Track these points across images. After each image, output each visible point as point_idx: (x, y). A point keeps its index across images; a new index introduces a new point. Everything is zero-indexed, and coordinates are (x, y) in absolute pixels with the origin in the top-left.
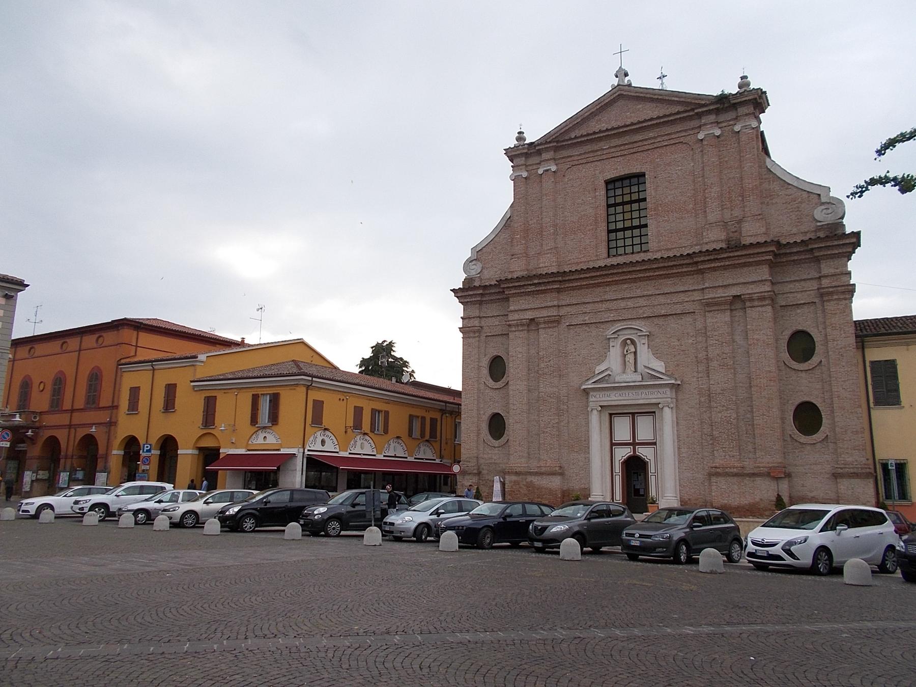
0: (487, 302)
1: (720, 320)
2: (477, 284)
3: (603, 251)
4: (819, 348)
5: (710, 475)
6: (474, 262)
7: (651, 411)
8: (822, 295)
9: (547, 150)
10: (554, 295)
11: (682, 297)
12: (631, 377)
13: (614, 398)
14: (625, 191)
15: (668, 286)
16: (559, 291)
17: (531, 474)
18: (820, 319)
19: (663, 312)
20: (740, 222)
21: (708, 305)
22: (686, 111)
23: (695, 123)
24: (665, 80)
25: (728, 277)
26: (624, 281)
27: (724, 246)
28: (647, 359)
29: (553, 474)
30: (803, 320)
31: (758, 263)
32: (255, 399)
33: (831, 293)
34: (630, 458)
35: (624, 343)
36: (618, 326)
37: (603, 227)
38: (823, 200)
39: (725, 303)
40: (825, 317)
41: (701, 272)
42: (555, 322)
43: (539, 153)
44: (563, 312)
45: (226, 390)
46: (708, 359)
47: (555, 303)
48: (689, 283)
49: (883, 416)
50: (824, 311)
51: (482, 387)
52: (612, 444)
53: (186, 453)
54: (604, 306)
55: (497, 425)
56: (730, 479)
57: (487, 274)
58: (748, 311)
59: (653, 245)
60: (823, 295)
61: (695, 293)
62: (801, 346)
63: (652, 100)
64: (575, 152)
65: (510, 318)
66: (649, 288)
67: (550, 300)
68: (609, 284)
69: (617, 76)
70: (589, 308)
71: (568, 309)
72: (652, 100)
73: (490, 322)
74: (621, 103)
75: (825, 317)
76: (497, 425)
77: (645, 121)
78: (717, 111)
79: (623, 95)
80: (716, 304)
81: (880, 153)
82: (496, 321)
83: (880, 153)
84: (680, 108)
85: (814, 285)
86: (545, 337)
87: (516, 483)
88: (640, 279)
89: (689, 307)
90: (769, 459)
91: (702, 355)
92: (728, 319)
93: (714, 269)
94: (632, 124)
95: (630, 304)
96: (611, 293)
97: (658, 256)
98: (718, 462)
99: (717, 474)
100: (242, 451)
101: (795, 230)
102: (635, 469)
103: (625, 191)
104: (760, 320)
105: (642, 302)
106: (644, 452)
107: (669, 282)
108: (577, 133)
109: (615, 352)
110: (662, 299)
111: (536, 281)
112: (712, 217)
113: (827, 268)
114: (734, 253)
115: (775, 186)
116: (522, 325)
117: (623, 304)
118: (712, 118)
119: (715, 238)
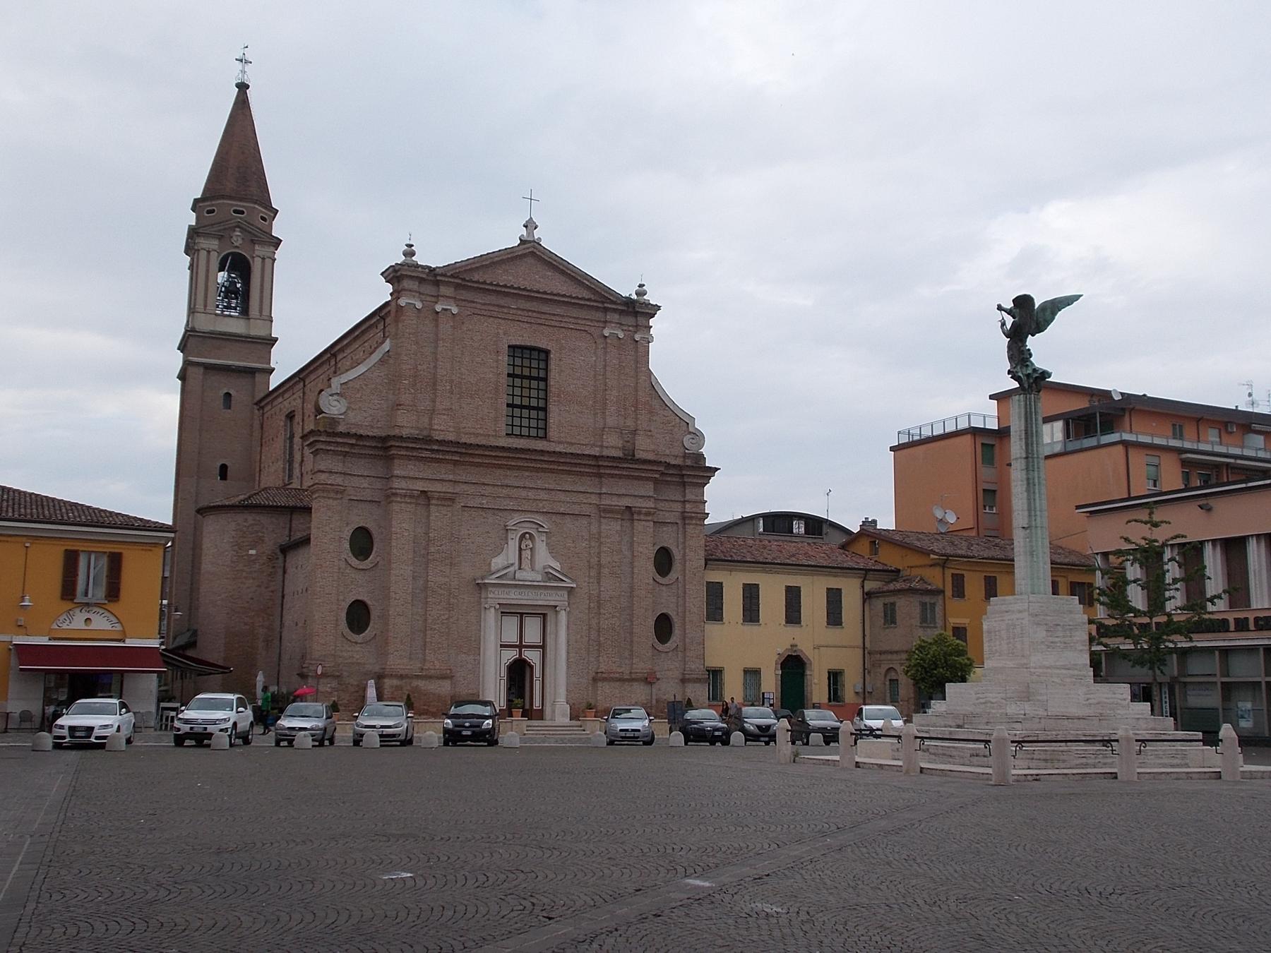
1: (612, 527)
2: (341, 429)
3: (503, 429)
4: (677, 566)
5: (595, 680)
6: (336, 397)
8: (684, 518)
9: (448, 284)
10: (450, 467)
11: (581, 497)
12: (527, 575)
13: (514, 597)
14: (530, 365)
15: (568, 483)
16: (455, 463)
17: (418, 677)
18: (681, 540)
19: (562, 510)
20: (634, 432)
21: (604, 511)
22: (589, 300)
23: (599, 315)
24: (248, 68)
25: (621, 487)
26: (527, 469)
27: (619, 454)
28: (544, 557)
29: (443, 677)
30: (668, 538)
31: (647, 479)
32: (71, 560)
33: (691, 518)
34: (516, 661)
35: (523, 536)
36: (518, 518)
37: (505, 399)
38: (691, 429)
39: (617, 512)
40: (685, 537)
41: (600, 476)
42: (449, 500)
43: (437, 283)
44: (458, 489)
46: (600, 565)
47: (451, 477)
48: (587, 485)
49: (712, 629)
51: (343, 565)
52: (543, 647)
56: (613, 684)
57: (354, 418)
58: (636, 523)
59: (553, 433)
61: (593, 496)
62: (664, 561)
63: (563, 273)
64: (480, 298)
65: (396, 484)
66: (549, 481)
67: (444, 472)
68: (510, 468)
69: (526, 226)
70: (489, 490)
72: (563, 273)
73: (356, 482)
74: (530, 260)
75: (685, 537)
76: (358, 616)
77: (558, 295)
78: (621, 312)
80: (611, 511)
81: (243, 87)
82: (365, 483)
83: (243, 87)
84: (586, 294)
85: (678, 507)
86: (438, 515)
88: (544, 470)
89: (586, 510)
90: (641, 667)
91: (594, 560)
92: (619, 528)
93: (612, 476)
94: (545, 293)
95: (531, 494)
96: (512, 478)
98: (603, 668)
99: (604, 679)
100: (43, 641)
101: (668, 452)
102: (518, 674)
103: (530, 365)
104: (644, 529)
105: (543, 495)
106: (532, 656)
107: (570, 478)
108: (476, 277)
109: (513, 545)
110: (562, 497)
111: (435, 447)
112: (611, 421)
114: (627, 464)
115: (655, 403)
116: (411, 497)
117: (523, 493)
118: (616, 317)
119: (613, 445)
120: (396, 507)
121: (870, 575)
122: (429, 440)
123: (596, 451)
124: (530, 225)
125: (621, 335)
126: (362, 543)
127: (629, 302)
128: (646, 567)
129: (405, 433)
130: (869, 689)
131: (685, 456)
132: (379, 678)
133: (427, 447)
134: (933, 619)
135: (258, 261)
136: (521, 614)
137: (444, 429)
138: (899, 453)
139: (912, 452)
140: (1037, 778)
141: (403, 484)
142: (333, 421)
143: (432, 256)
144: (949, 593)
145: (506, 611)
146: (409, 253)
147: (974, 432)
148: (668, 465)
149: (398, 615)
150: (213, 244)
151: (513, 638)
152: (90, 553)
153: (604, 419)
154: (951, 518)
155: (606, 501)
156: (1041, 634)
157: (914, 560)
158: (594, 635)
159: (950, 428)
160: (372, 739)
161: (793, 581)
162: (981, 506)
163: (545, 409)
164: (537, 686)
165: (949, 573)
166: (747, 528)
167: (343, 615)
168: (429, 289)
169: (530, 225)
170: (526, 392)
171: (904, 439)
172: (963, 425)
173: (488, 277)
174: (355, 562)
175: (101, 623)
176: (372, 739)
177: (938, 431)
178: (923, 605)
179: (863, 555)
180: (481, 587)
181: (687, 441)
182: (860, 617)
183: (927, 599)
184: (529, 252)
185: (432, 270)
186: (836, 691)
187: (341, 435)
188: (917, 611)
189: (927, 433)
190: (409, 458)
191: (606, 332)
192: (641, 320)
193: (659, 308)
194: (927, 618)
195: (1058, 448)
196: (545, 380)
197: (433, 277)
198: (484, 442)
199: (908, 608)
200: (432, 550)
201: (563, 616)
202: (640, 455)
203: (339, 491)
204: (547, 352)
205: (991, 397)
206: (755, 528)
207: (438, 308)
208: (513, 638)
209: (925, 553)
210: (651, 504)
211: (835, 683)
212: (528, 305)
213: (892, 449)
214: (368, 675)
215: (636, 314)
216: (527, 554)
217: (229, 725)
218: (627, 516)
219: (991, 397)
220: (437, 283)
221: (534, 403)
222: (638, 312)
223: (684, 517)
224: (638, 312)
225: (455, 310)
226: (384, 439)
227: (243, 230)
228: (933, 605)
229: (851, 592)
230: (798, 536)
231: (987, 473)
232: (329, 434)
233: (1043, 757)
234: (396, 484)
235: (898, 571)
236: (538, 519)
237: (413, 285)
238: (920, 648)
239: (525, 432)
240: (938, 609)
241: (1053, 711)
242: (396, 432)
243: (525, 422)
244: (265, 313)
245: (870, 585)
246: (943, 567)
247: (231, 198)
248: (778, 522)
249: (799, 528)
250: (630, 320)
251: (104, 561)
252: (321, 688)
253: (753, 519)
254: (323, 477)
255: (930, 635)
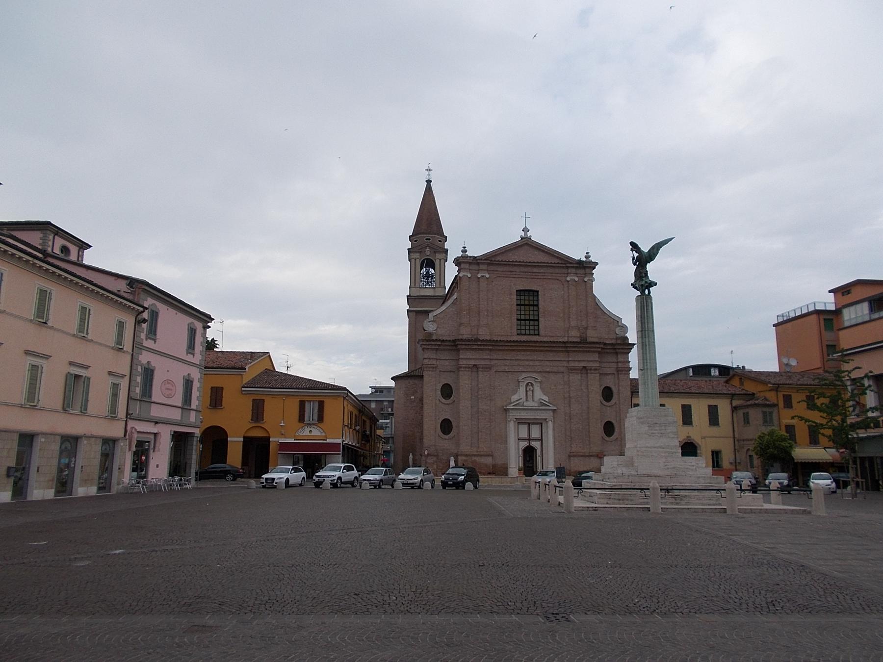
0: (441, 350)
1: (576, 378)
2: (434, 338)
3: (515, 332)
4: (615, 396)
5: (570, 456)
7: (540, 423)
9: (483, 263)
12: (530, 404)
13: (523, 415)
14: (528, 300)
15: (551, 356)
17: (475, 455)
20: (586, 328)
21: (571, 369)
23: (565, 271)
25: (580, 357)
27: (578, 340)
28: (539, 394)
30: (610, 382)
31: (594, 352)
32: (302, 405)
35: (527, 384)
36: (524, 375)
37: (515, 317)
41: (568, 352)
42: (488, 368)
45: (273, 395)
46: (570, 397)
48: (562, 356)
50: (618, 379)
52: (541, 440)
53: (235, 442)
54: (517, 363)
55: (446, 426)
57: (440, 332)
59: (542, 332)
60: (619, 371)
62: (607, 394)
63: (543, 251)
64: (500, 269)
65: (461, 362)
68: (519, 351)
70: (508, 362)
71: (496, 362)
72: (543, 251)
74: (526, 247)
76: (446, 426)
78: (577, 268)
79: (526, 243)
81: (429, 182)
83: (429, 182)
84: (557, 261)
85: (614, 365)
86: (483, 376)
87: (466, 461)
88: (537, 351)
89: (561, 369)
90: (595, 449)
91: (567, 395)
93: (574, 351)
95: (531, 363)
97: (545, 340)
98: (574, 450)
99: (574, 456)
100: (292, 441)
102: (529, 453)
103: (528, 300)
104: (594, 378)
105: (537, 363)
106: (536, 445)
108: (498, 258)
109: (522, 389)
110: (548, 363)
112: (573, 323)
113: (621, 358)
114: (583, 345)
117: (527, 363)
118: (573, 270)
119: (574, 335)
120: (461, 373)
121: (735, 397)
122: (477, 340)
123: (566, 339)
124: (526, 230)
125: (577, 279)
126: (447, 391)
127: (580, 262)
128: (596, 396)
129: (465, 337)
130: (738, 461)
131: (617, 339)
132: (456, 457)
133: (476, 344)
134: (771, 420)
135: (438, 261)
136: (529, 423)
137: (484, 334)
138: (780, 327)
139: (786, 327)
140: (596, 509)
141: (465, 362)
142: (430, 334)
143: (475, 251)
144: (781, 404)
145: (520, 422)
146: (464, 251)
147: (818, 312)
148: (605, 344)
149: (464, 425)
150: (417, 255)
151: (526, 436)
152: (310, 401)
153: (569, 322)
154: (793, 363)
155: (572, 364)
156: (645, 428)
157: (761, 388)
158: (568, 434)
159: (805, 311)
160: (327, 484)
161: (686, 401)
162: (825, 354)
163: (538, 320)
164: (539, 459)
165: (780, 395)
166: (682, 375)
167: (439, 426)
168: (474, 267)
169: (526, 230)
170: (527, 313)
171: (781, 320)
172: (811, 309)
173: (499, 258)
174: (443, 400)
175: (316, 432)
176: (327, 484)
177: (798, 313)
178: (764, 413)
179: (735, 386)
180: (506, 410)
181: (618, 330)
182: (730, 420)
183: (767, 410)
184: (526, 243)
185: (475, 258)
186: (717, 462)
187: (433, 340)
188: (760, 416)
189: (792, 315)
190: (467, 349)
191: (568, 279)
192: (588, 270)
193: (597, 264)
194: (767, 419)
195: (867, 318)
196: (537, 305)
197: (475, 261)
198: (505, 339)
199: (755, 415)
200: (480, 393)
201: (550, 424)
202: (590, 340)
203: (434, 368)
204: (538, 292)
205: (830, 292)
206: (687, 374)
207: (479, 276)
208: (526, 436)
209: (765, 383)
210: (597, 365)
211: (717, 457)
212: (526, 270)
213: (774, 325)
214: (451, 455)
215: (585, 268)
216: (530, 393)
217: (336, 478)
218: (584, 371)
219: (830, 292)
220: (478, 264)
221: (532, 317)
222: (586, 267)
223: (619, 371)
224: (586, 267)
225: (488, 276)
226: (454, 341)
227: (430, 247)
228: (771, 413)
229: (724, 408)
230: (714, 377)
231: (828, 336)
232: (427, 341)
233: (617, 497)
234: (461, 362)
235: (753, 394)
236: (535, 375)
237: (467, 266)
238: (760, 437)
239: (532, 332)
240: (775, 415)
241: (642, 471)
242: (460, 337)
243: (527, 328)
244: (442, 284)
245: (735, 403)
246: (777, 391)
247: (423, 233)
248: (702, 370)
249: (715, 372)
250: (582, 271)
251: (317, 404)
252: (428, 461)
253: (686, 369)
254: (426, 361)
255: (766, 430)
